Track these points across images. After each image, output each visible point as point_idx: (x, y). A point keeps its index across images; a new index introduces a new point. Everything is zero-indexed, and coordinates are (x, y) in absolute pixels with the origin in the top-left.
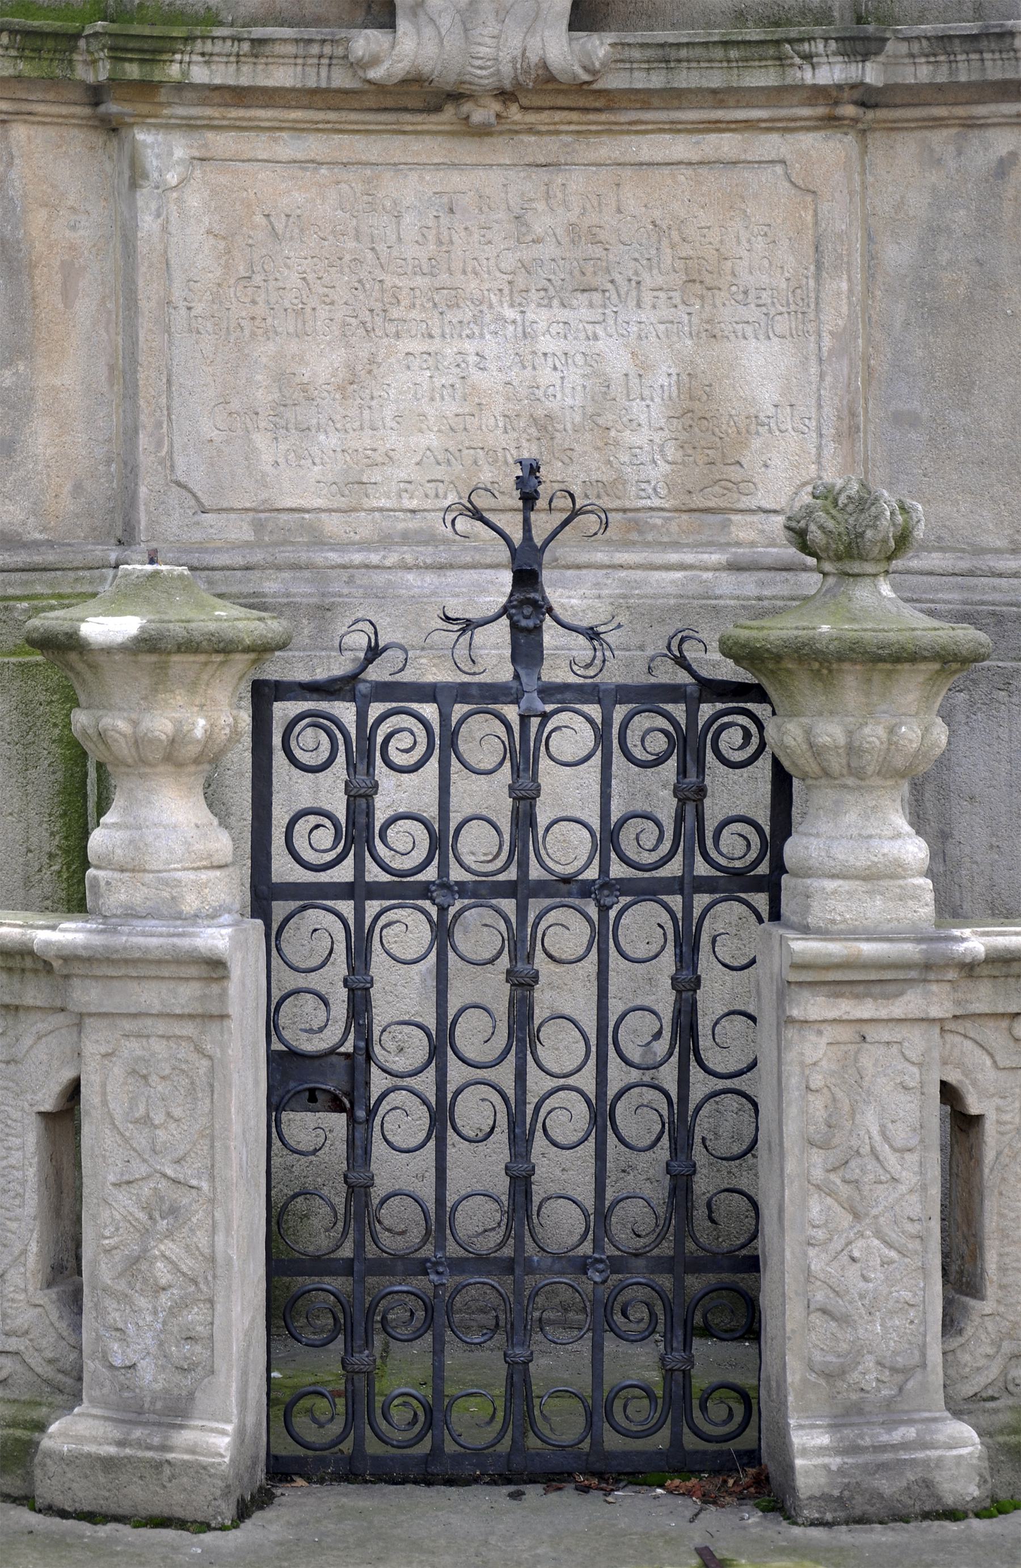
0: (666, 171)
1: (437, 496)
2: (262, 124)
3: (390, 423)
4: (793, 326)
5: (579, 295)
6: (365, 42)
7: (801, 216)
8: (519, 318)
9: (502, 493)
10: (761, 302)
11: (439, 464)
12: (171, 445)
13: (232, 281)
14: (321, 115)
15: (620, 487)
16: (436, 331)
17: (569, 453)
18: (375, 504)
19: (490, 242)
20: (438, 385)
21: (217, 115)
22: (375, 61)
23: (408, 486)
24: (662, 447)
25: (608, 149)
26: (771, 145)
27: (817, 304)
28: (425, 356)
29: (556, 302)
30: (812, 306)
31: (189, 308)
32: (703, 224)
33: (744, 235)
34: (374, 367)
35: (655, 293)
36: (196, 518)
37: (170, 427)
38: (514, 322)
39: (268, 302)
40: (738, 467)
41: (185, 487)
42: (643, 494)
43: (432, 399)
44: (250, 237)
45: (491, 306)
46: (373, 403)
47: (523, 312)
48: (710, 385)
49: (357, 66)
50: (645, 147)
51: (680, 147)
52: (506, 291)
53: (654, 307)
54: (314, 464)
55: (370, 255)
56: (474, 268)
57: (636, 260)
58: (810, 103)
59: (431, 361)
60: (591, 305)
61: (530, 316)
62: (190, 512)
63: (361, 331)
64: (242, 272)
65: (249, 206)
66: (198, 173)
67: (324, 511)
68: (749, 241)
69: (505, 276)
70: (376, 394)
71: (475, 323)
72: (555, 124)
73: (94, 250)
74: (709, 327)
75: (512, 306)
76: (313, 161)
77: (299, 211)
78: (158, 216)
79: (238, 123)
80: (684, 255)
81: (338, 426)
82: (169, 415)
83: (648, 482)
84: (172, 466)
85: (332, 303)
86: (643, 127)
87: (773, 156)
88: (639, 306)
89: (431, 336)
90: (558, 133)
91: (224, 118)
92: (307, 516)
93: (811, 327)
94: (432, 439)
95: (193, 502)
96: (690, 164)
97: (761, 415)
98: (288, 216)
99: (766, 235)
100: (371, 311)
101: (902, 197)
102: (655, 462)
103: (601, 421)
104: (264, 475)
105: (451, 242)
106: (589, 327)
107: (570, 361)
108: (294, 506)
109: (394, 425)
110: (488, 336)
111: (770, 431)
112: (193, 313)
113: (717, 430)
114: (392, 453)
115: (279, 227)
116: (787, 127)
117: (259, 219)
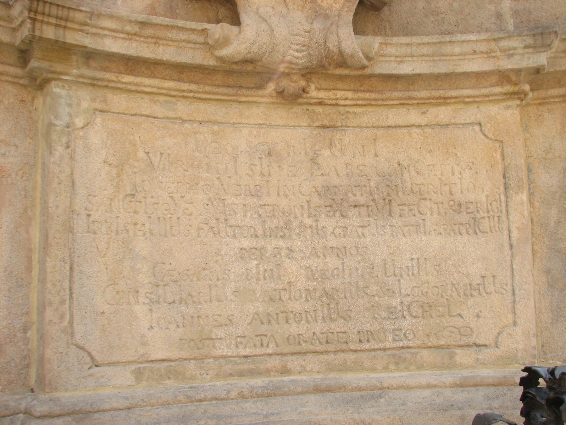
0: (405, 130)
1: (262, 345)
2: (146, 89)
3: (230, 297)
4: (492, 225)
5: (352, 209)
6: (218, 30)
7: (492, 156)
8: (314, 225)
9: (305, 342)
10: (469, 211)
11: (262, 323)
12: (72, 316)
13: (121, 197)
14: (185, 86)
15: (382, 334)
16: (260, 233)
17: (349, 313)
18: (219, 353)
19: (294, 175)
20: (262, 269)
21: (114, 78)
22: (226, 42)
23: (242, 340)
24: (409, 306)
25: (369, 116)
26: (470, 114)
27: (507, 211)
28: (254, 251)
29: (338, 214)
30: (504, 211)
31: (89, 215)
32: (430, 163)
33: (457, 169)
34: (219, 258)
35: (401, 207)
36: (91, 371)
37: (71, 303)
38: (311, 227)
39: (146, 213)
40: (459, 318)
41: (82, 348)
42: (397, 338)
43: (258, 279)
44: (134, 167)
45: (296, 217)
46: (219, 283)
47: (316, 220)
48: (439, 265)
49: (210, 47)
50: (391, 116)
51: (413, 116)
52: (306, 206)
53: (401, 216)
54: (178, 326)
55: (217, 182)
56: (285, 192)
57: (388, 186)
58: (499, 83)
59: (258, 253)
60: (360, 215)
61: (321, 223)
62: (86, 367)
63: (211, 235)
64: (128, 190)
65: (135, 145)
66: (99, 120)
67: (185, 359)
68: (460, 173)
69: (304, 197)
70: (221, 276)
71: (286, 228)
72: (337, 99)
73: (20, 173)
74: (436, 228)
75: (309, 217)
76: (180, 118)
77: (169, 151)
78: (68, 147)
79: (129, 87)
80: (419, 182)
81: (195, 299)
82: (71, 294)
83: (266, 336)
84: (72, 333)
85: (191, 214)
86: (391, 103)
87: (472, 120)
88: (390, 215)
89: (257, 237)
90: (337, 105)
91: (119, 82)
92: (173, 364)
93: (505, 226)
94: (259, 307)
95: (88, 359)
96: (419, 126)
97: (474, 283)
98: (162, 154)
99: (471, 168)
100: (217, 219)
101: (550, 145)
102: (403, 316)
103: (368, 291)
104: (143, 336)
105: (270, 175)
106: (360, 230)
107: (348, 253)
108: (164, 358)
109: (233, 298)
110: (294, 237)
111: (480, 293)
112: (92, 219)
113: (444, 294)
114: (231, 318)
115: (156, 160)
116: (487, 99)
117: (141, 154)
